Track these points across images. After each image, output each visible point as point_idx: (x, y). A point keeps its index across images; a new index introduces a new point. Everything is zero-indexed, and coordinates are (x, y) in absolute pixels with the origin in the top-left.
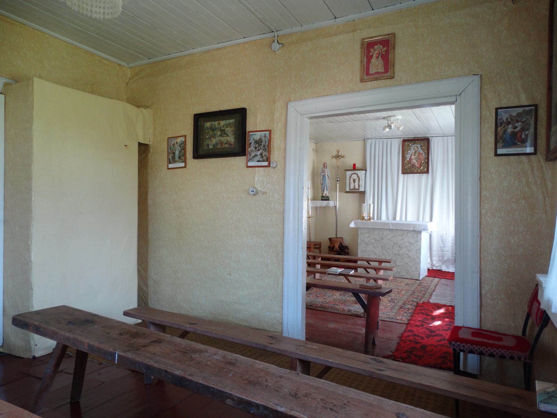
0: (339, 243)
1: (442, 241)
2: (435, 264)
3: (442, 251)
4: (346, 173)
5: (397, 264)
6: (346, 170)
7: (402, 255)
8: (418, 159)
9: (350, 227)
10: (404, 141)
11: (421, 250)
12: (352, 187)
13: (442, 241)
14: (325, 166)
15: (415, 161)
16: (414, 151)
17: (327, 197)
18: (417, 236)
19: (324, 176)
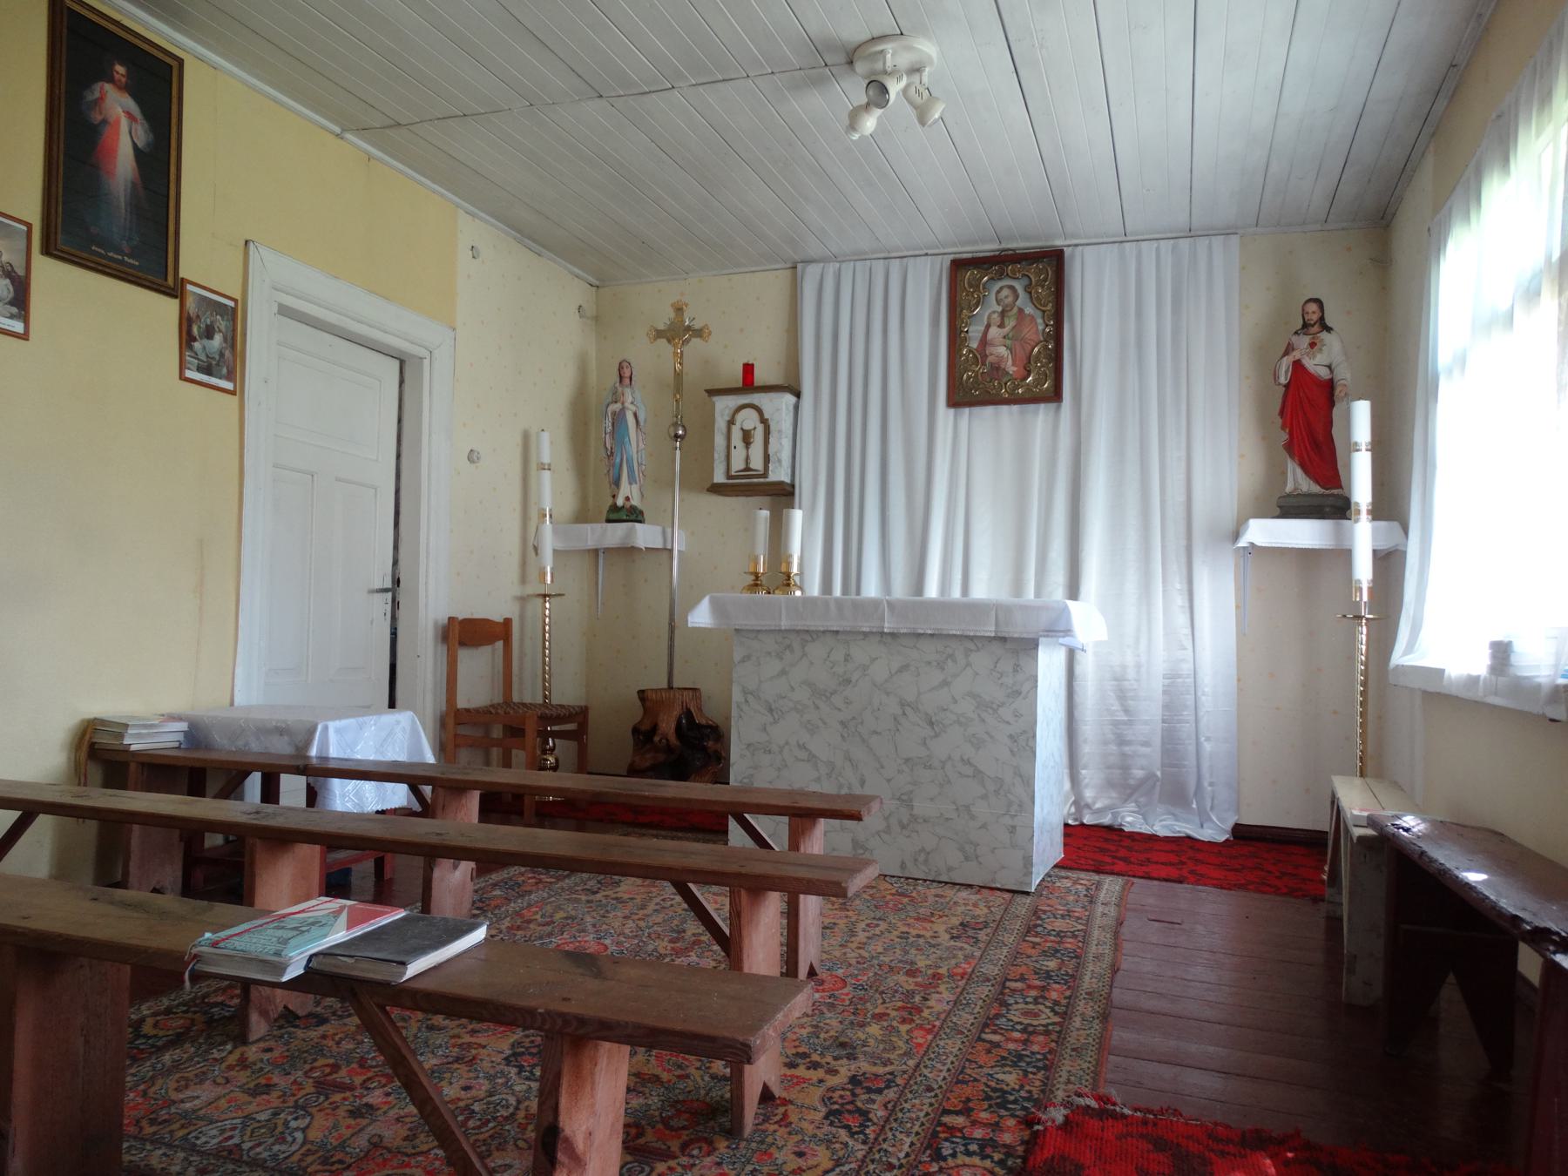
0: (676, 712)
1: (1122, 695)
2: (1089, 801)
3: (1121, 741)
4: (713, 405)
5: (915, 812)
6: (712, 392)
7: (943, 763)
8: (1012, 339)
9: (690, 625)
10: (958, 265)
11: (1034, 736)
12: (737, 464)
13: (1122, 695)
14: (624, 375)
15: (1002, 351)
16: (1000, 309)
17: (633, 510)
18: (1016, 669)
19: (618, 418)
